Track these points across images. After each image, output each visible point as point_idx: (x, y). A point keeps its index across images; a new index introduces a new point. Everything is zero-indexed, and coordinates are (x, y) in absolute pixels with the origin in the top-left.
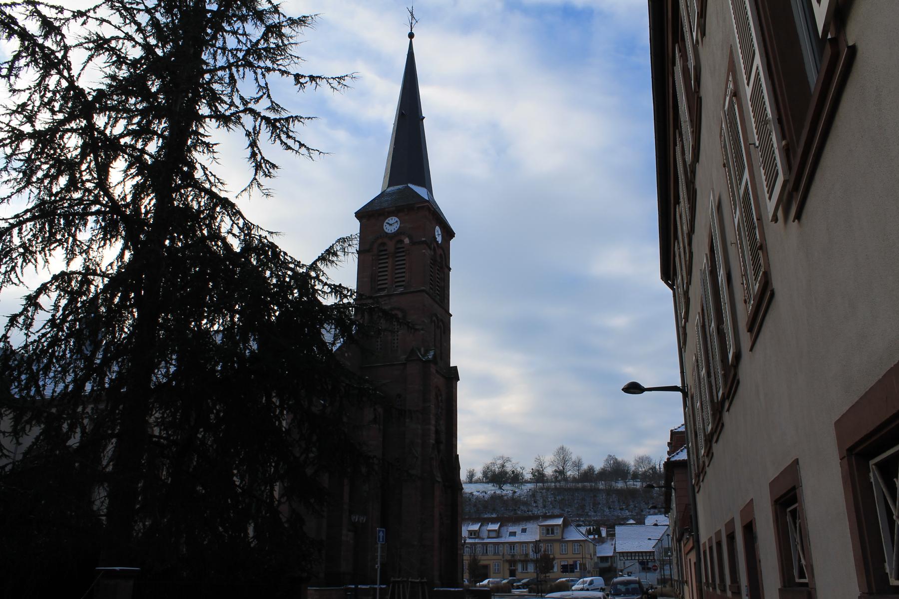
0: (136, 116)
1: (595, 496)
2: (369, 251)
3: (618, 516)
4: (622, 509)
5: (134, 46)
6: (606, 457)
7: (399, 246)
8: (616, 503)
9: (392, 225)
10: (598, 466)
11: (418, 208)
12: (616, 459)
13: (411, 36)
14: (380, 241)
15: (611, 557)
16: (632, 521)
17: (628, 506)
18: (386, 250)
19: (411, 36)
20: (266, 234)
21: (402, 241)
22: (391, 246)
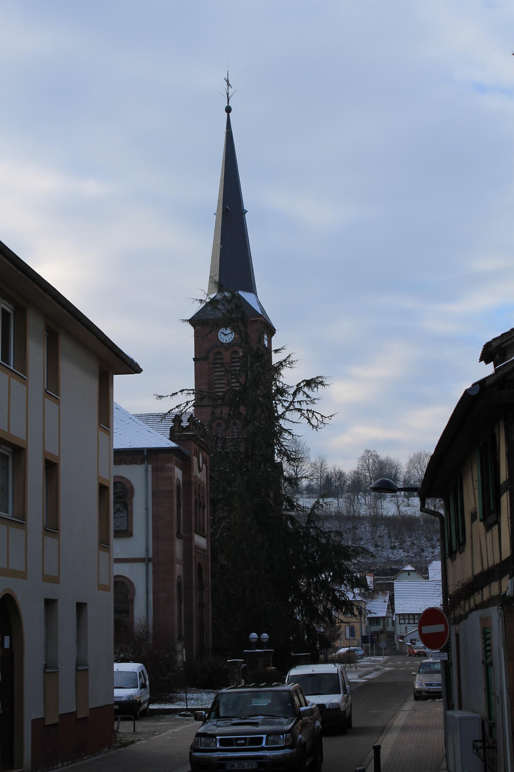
0: (314, 511)
1: (355, 528)
2: (205, 359)
3: (388, 559)
4: (393, 548)
5: (409, 574)
6: (361, 453)
7: (234, 356)
8: (386, 539)
9: (226, 336)
10: (349, 466)
11: (252, 321)
12: (377, 457)
13: (228, 110)
14: (215, 350)
15: (383, 618)
16: (409, 568)
19: (228, 110)
21: (236, 352)
22: (227, 356)
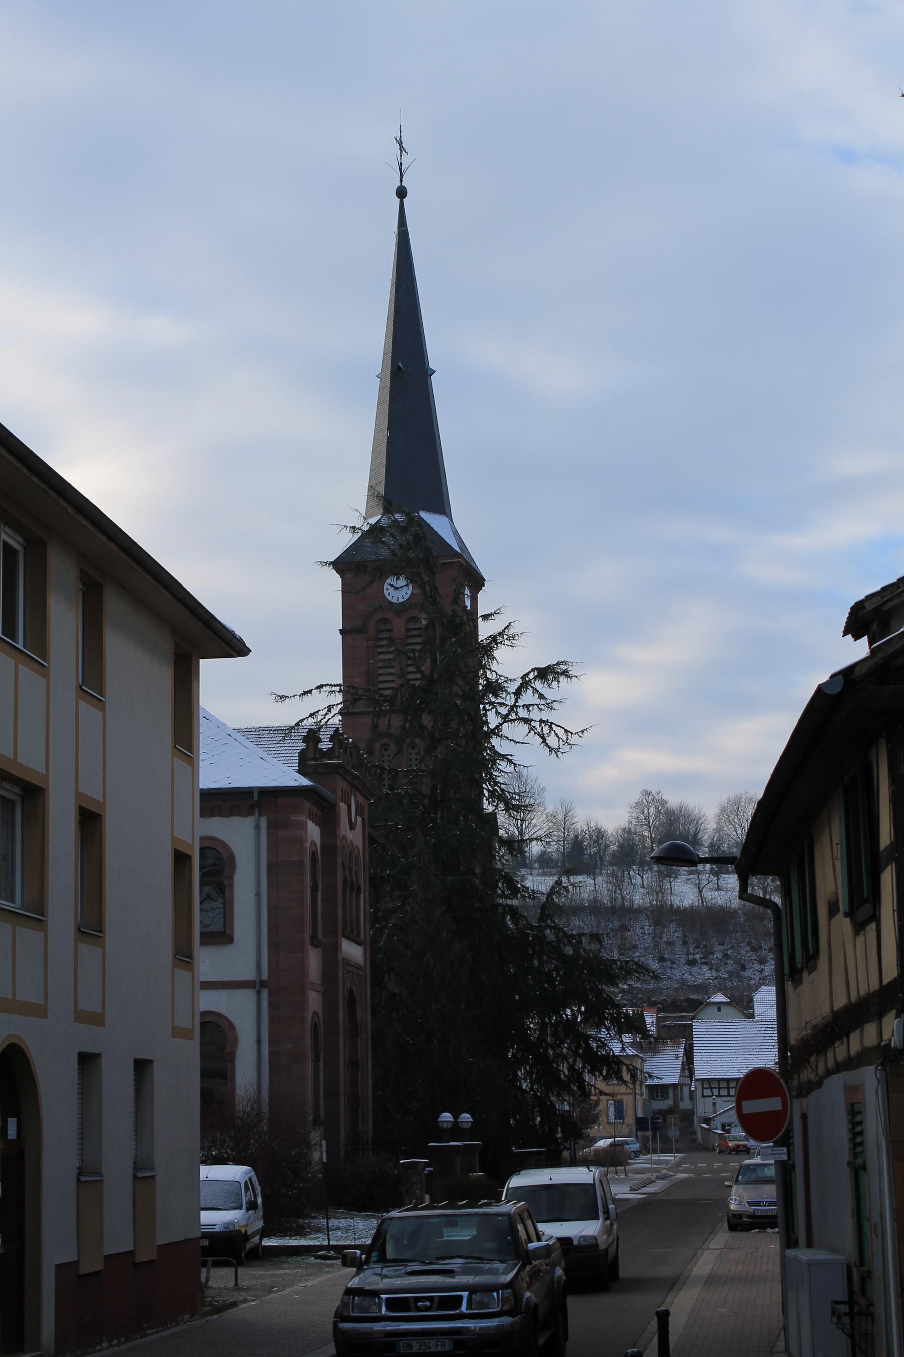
0: (552, 899)
1: (624, 928)
2: (360, 631)
3: (683, 982)
4: (692, 963)
5: (719, 1010)
6: (636, 796)
7: (412, 626)
8: (678, 947)
9: (398, 590)
10: (614, 820)
12: (663, 803)
13: (402, 193)
15: (674, 1086)
16: (720, 998)
17: (707, 953)
18: (391, 630)
19: (402, 193)
20: (311, 720)
21: (415, 619)
22: (399, 625)
